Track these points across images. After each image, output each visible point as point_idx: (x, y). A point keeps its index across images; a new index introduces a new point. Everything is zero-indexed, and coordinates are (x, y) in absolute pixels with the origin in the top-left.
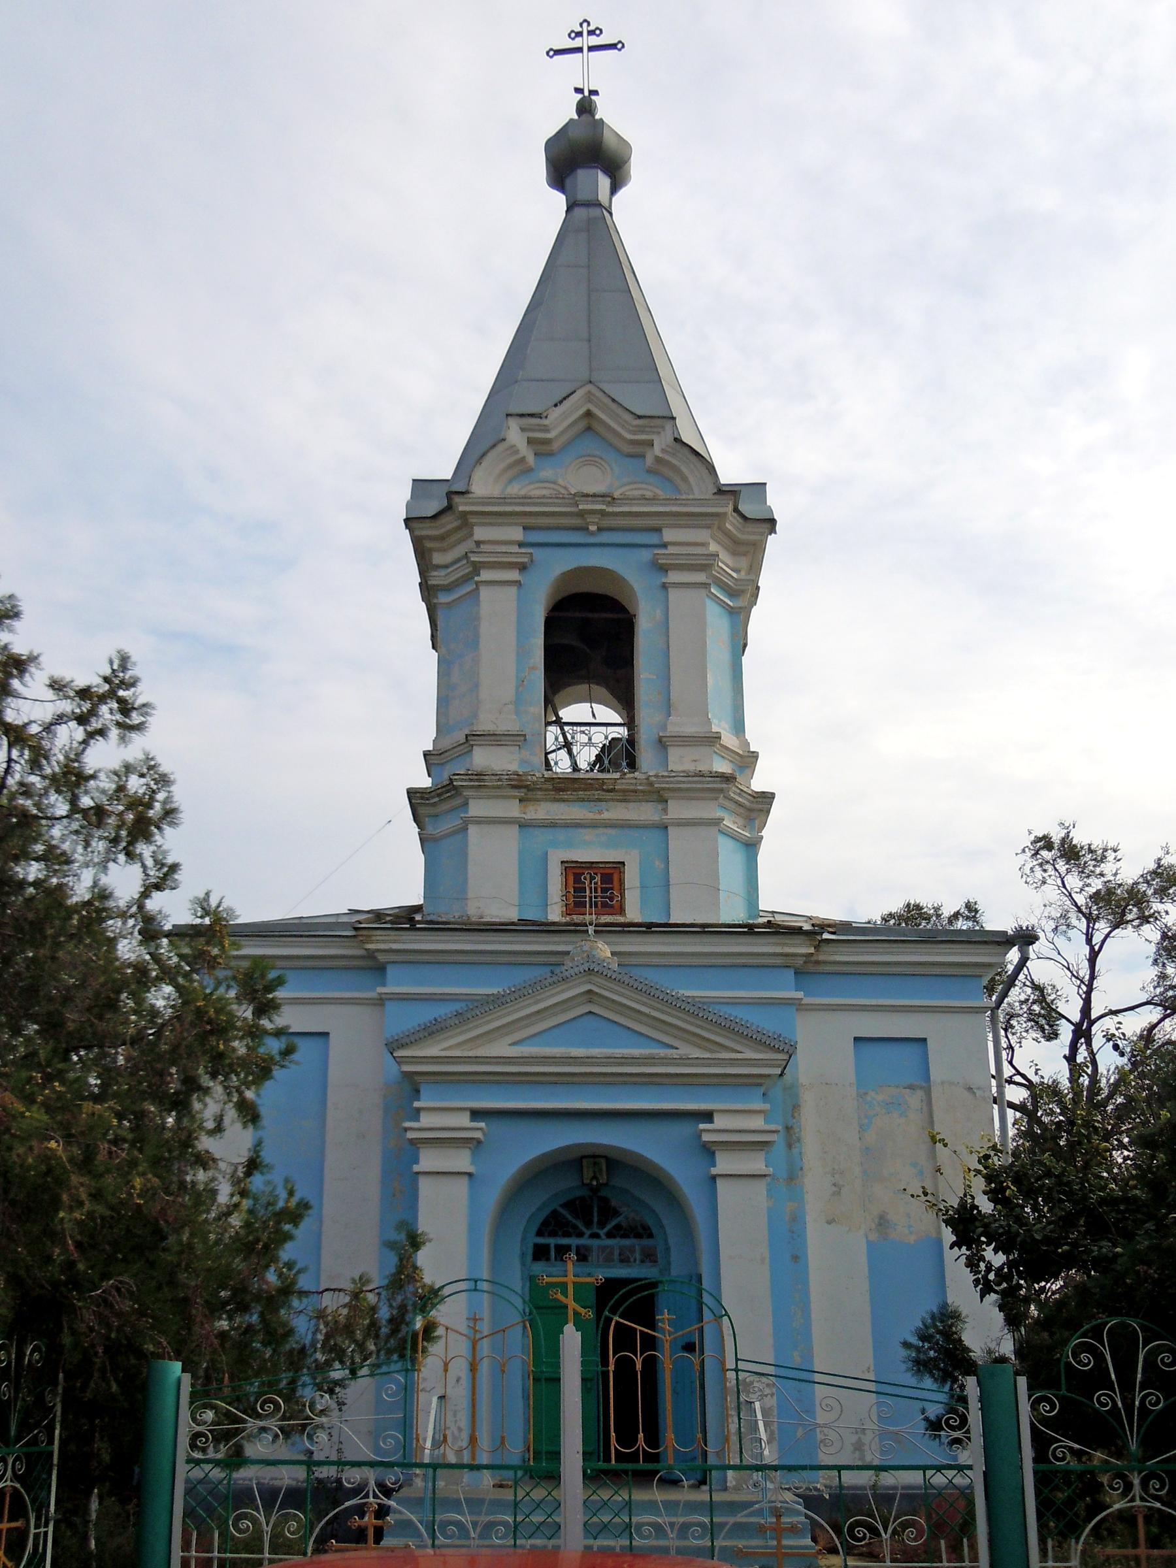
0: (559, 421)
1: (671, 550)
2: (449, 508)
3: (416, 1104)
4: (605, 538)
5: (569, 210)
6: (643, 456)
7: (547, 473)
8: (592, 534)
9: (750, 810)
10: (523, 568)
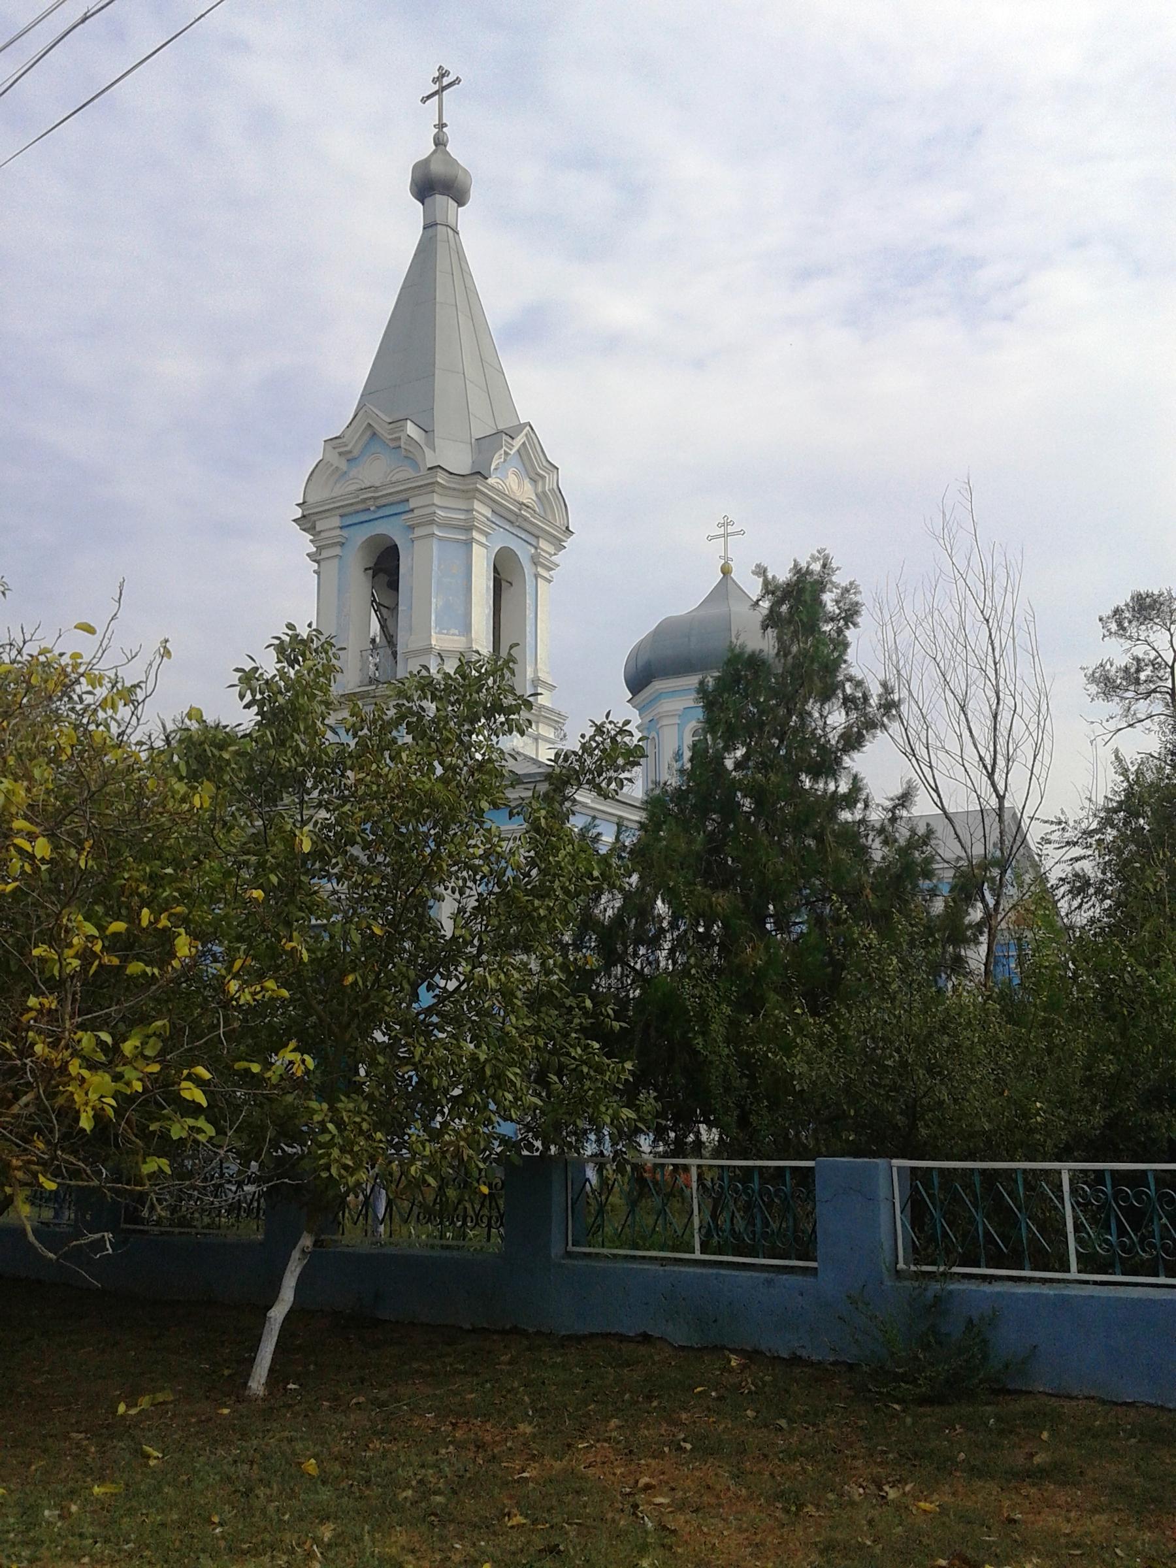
4: (380, 513)
8: (374, 512)
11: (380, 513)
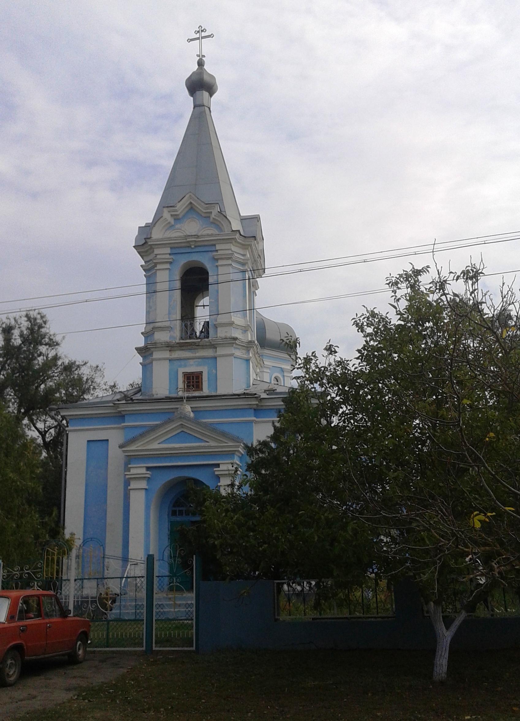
0: (181, 207)
1: (220, 252)
2: (146, 243)
3: (129, 466)
4: (197, 250)
5: (194, 108)
6: (209, 217)
7: (178, 226)
8: (192, 248)
9: (247, 347)
10: (171, 263)
11: (197, 250)
